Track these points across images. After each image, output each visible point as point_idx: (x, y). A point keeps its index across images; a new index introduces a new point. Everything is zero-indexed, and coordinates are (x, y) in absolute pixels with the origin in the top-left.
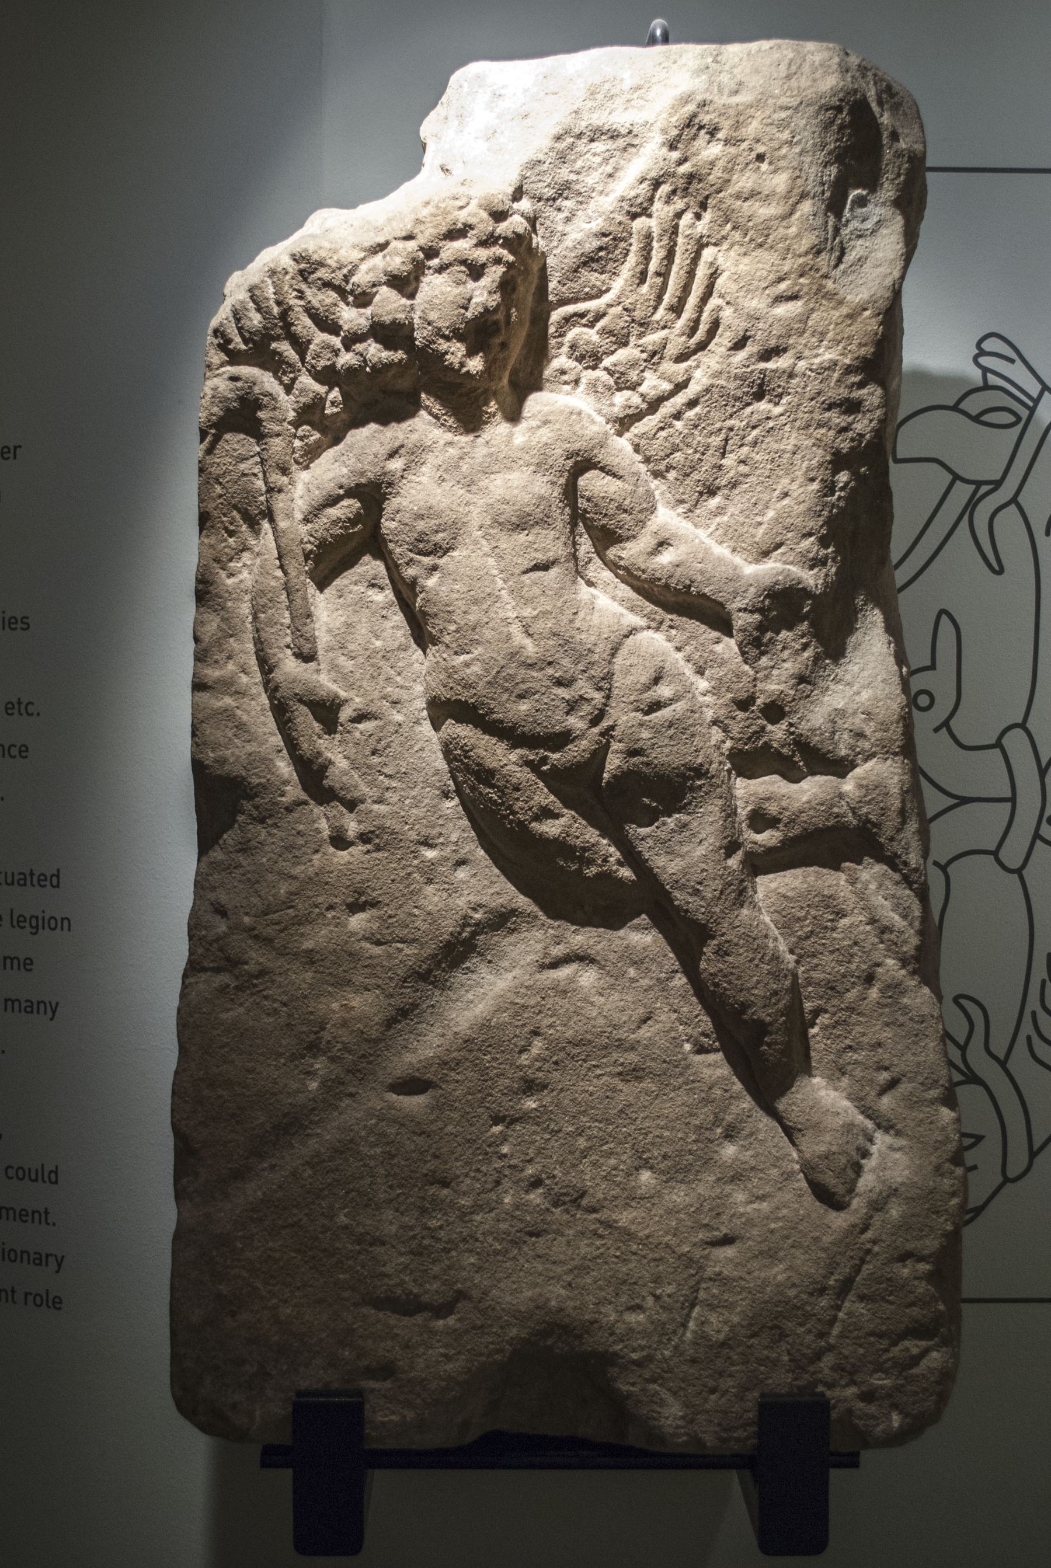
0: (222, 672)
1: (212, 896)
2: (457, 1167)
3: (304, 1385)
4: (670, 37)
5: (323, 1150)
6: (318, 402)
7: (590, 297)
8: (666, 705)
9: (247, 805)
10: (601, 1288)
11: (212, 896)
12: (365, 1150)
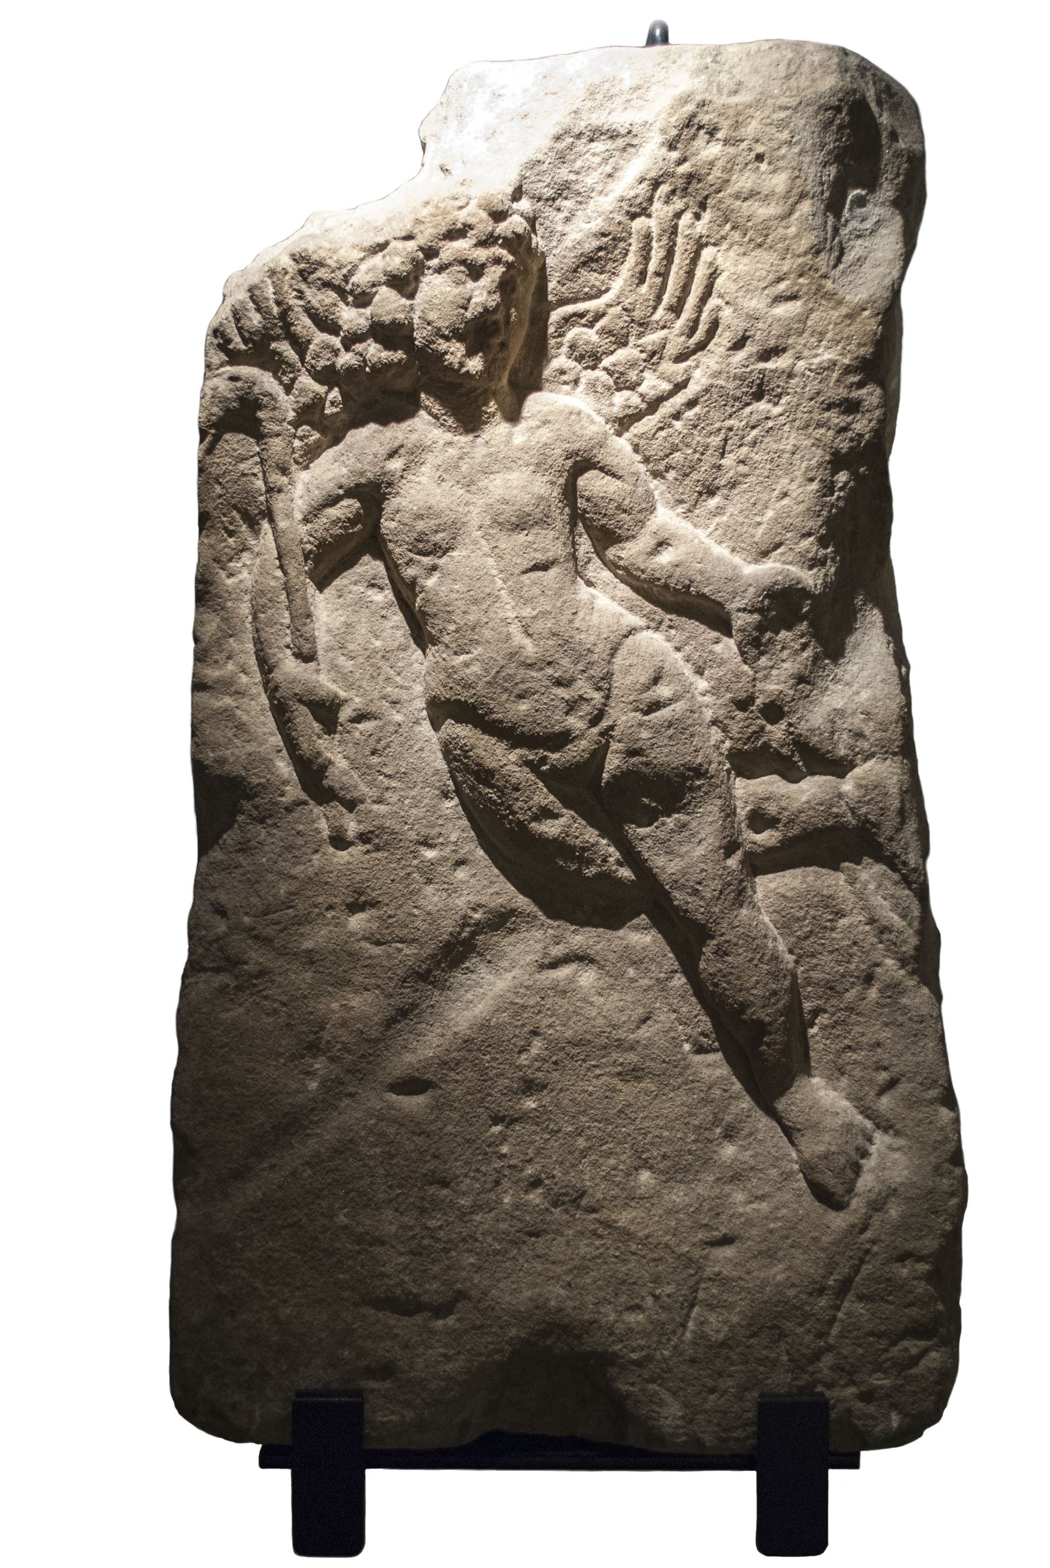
1: (212, 896)
2: (457, 1167)
3: (303, 1385)
5: (322, 1150)
7: (589, 297)
8: (665, 705)
9: (247, 805)
10: (600, 1288)
11: (212, 896)
12: (364, 1150)
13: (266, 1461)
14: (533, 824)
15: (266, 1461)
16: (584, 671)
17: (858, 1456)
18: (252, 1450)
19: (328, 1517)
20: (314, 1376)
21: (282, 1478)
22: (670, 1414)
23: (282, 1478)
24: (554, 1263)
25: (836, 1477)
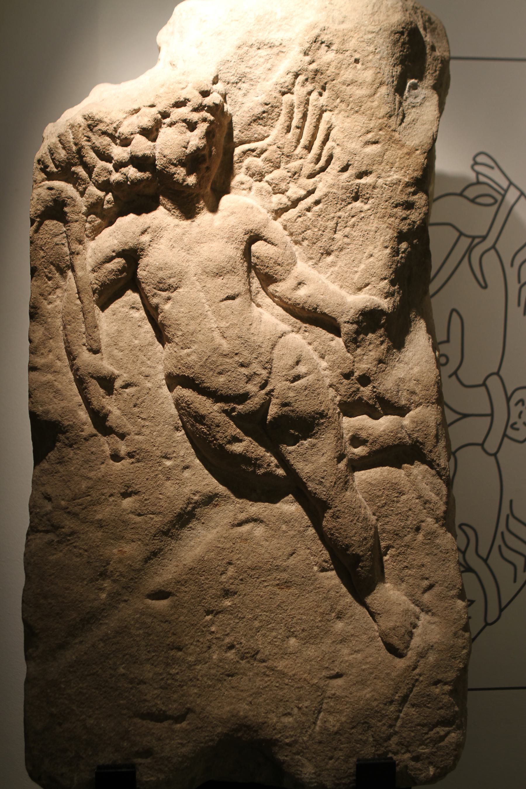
1: (42, 489)
3: (101, 762)
8: (303, 377)
9: (62, 437)
11: (42, 489)
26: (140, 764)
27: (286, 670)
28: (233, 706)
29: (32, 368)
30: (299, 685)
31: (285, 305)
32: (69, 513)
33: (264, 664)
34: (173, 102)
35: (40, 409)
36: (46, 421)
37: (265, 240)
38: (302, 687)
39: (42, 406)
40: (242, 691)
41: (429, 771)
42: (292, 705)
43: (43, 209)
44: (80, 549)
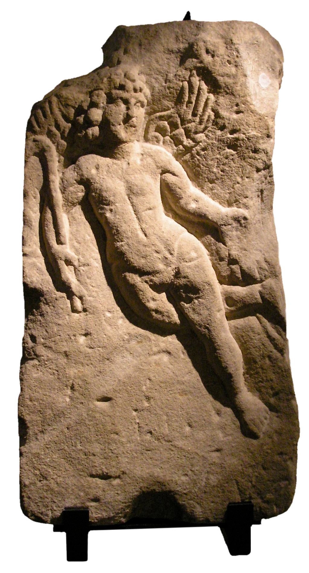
0: (61, 206)
1: (29, 332)
2: (120, 427)
3: (67, 505)
4: (25, 257)
5: (72, 423)
6: (89, 123)
7: (165, 110)
8: (195, 260)
9: (42, 299)
10: (172, 469)
11: (29, 332)
12: (87, 422)
13: (55, 530)
14: (77, 298)
15: (55, 530)
16: (41, 498)
17: (260, 521)
18: (51, 526)
19: (77, 551)
20: (71, 502)
21: (63, 536)
22: (198, 511)
23: (63, 536)
24: (156, 460)
25: (254, 528)
26: (91, 506)
27: (184, 447)
28: (150, 470)
29: (24, 255)
30: (192, 457)
31: (180, 213)
32: (46, 346)
33: (171, 443)
34: (284, 70)
35: (28, 280)
36: (31, 288)
37: (171, 173)
38: (194, 458)
39: (29, 278)
40: (156, 460)
41: (273, 510)
42: (188, 469)
43: (105, 517)
44: (53, 369)
